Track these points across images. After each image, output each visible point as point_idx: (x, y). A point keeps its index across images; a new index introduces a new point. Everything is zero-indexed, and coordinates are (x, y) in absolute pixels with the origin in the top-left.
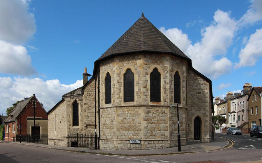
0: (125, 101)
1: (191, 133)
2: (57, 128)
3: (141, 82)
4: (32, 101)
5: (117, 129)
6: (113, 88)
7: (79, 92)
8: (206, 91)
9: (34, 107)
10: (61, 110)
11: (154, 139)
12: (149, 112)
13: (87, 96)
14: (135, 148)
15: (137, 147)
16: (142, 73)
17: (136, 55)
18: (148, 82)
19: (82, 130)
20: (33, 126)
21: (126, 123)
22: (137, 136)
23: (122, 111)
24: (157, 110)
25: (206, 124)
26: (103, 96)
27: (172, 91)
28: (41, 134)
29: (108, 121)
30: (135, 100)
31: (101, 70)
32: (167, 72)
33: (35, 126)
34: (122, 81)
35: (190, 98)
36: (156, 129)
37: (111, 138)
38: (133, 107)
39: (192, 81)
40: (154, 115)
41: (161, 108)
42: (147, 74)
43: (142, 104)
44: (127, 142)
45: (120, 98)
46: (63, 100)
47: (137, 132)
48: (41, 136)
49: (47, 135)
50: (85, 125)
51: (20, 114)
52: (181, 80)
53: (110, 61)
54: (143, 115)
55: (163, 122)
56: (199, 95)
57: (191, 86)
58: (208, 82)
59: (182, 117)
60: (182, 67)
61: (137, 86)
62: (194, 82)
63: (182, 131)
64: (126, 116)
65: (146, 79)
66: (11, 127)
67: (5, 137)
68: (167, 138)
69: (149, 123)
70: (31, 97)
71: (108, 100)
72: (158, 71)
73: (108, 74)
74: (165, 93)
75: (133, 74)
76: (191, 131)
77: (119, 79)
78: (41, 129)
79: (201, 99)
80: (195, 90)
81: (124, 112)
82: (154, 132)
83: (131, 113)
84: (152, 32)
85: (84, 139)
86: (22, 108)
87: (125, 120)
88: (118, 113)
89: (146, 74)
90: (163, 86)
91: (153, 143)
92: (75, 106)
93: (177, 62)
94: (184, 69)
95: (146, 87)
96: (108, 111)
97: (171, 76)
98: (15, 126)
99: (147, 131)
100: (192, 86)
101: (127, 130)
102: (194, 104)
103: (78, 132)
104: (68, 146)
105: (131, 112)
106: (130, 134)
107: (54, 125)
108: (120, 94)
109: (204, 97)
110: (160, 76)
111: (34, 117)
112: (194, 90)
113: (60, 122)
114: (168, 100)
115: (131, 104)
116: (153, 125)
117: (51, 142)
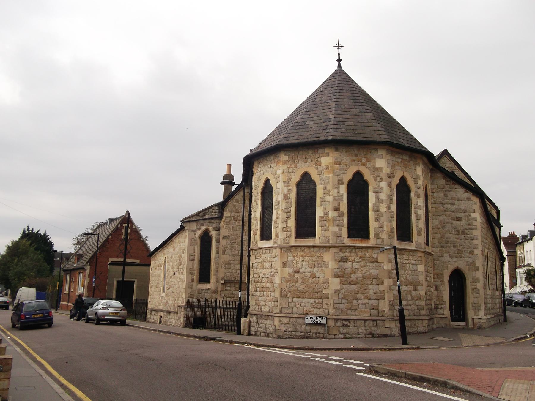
0: (299, 235)
1: (443, 306)
2: (167, 286)
3: (329, 199)
4: (122, 225)
5: (281, 292)
6: (275, 209)
7: (214, 213)
8: (473, 215)
9: (126, 239)
10: (178, 248)
11: (356, 316)
12: (344, 260)
13: (230, 221)
14: (316, 333)
15: (319, 333)
16: (330, 180)
17: (321, 148)
18: (343, 198)
19: (215, 292)
20: (121, 279)
21: (300, 281)
22: (321, 309)
23: (291, 255)
24: (361, 255)
25: (476, 285)
26: (258, 225)
27: (391, 217)
28: (134, 298)
29: (265, 274)
30: (318, 234)
31: (255, 174)
32: (382, 178)
33: (125, 280)
34: (293, 196)
35: (439, 228)
36: (359, 296)
37: (269, 312)
38: (312, 249)
39: (442, 195)
40: (356, 265)
41: (369, 251)
42: (341, 182)
43: (331, 242)
44: (301, 321)
45: (289, 230)
46: (182, 229)
47: (320, 300)
48: (134, 301)
49: (147, 300)
50: (223, 282)
51: (96, 252)
52: (413, 195)
53: (272, 158)
54: (332, 265)
55: (374, 280)
56: (458, 222)
57: (440, 205)
58: (477, 197)
59: (417, 270)
60: (413, 167)
61: (321, 206)
62: (445, 195)
63: (417, 301)
64: (299, 266)
65: (338, 192)
66: (76, 278)
67: (61, 303)
68: (383, 316)
69: (345, 283)
70: (121, 217)
71: (266, 235)
72: (363, 178)
73: (267, 181)
74: (377, 219)
75: (314, 184)
76: (442, 301)
77: (288, 193)
78: (135, 286)
79: (463, 232)
80: (448, 213)
81: (296, 258)
82: (355, 302)
83: (308, 261)
84: (355, 101)
85: (219, 312)
86: (102, 239)
87: (297, 275)
88: (285, 260)
89: (338, 184)
90: (374, 206)
91: (353, 324)
92: (206, 240)
93: (402, 159)
94: (419, 170)
95: (339, 208)
96: (265, 255)
97: (389, 185)
98: (84, 278)
99: (341, 299)
100: (442, 204)
101: (301, 295)
102: (447, 242)
103: (207, 296)
104: (187, 325)
105: (309, 259)
106: (308, 304)
107: (162, 279)
108: (289, 221)
109: (470, 227)
110: (368, 186)
111: (125, 260)
112: (447, 213)
113: (174, 274)
114: (384, 236)
115: (309, 242)
116: (353, 286)
117: (152, 317)
